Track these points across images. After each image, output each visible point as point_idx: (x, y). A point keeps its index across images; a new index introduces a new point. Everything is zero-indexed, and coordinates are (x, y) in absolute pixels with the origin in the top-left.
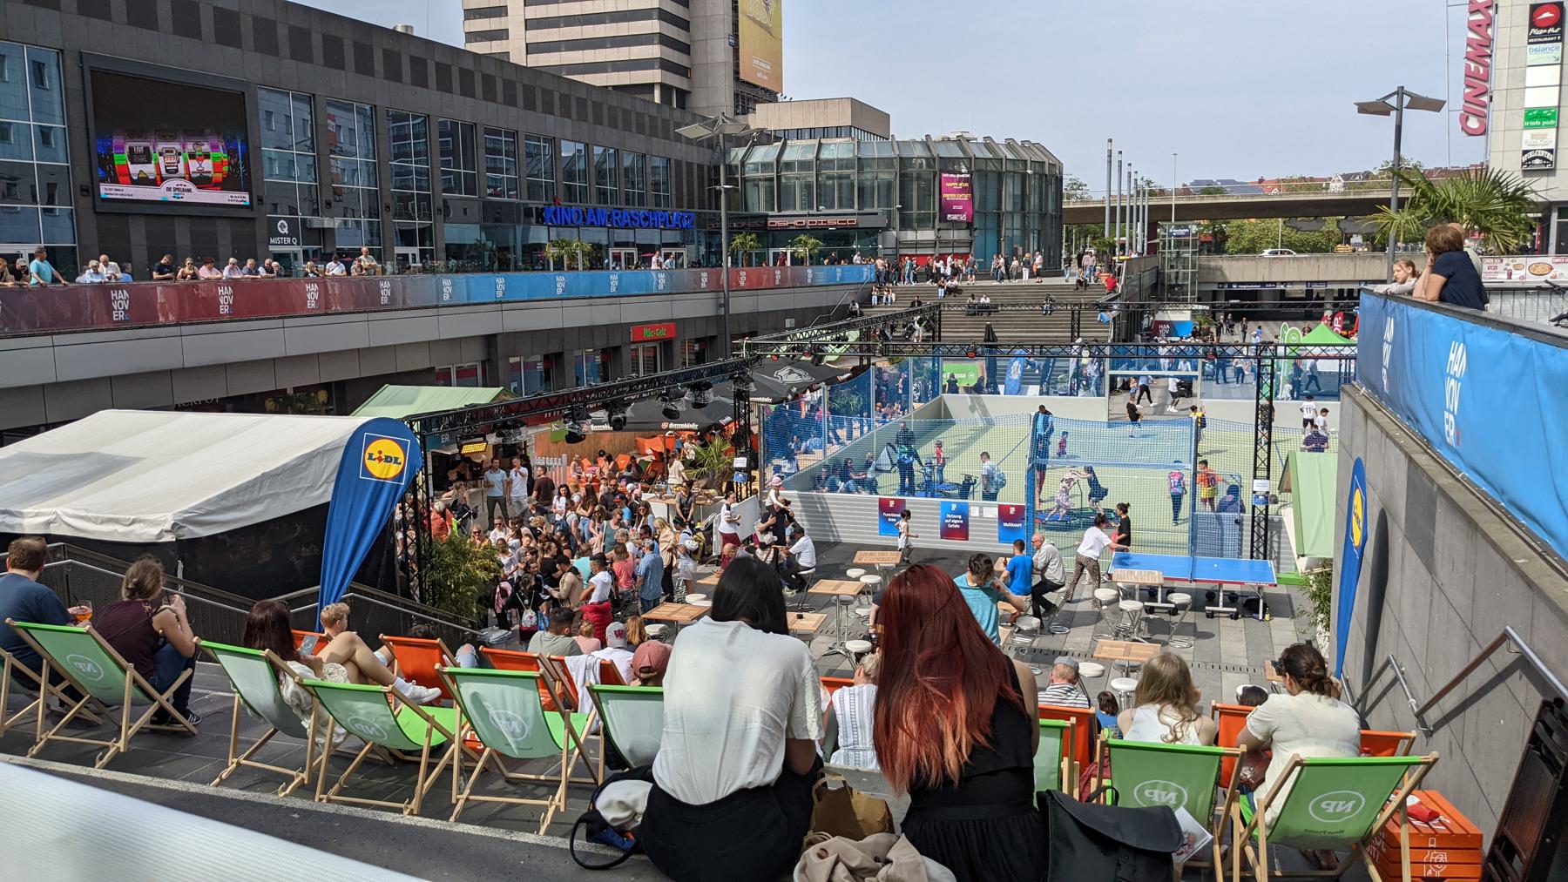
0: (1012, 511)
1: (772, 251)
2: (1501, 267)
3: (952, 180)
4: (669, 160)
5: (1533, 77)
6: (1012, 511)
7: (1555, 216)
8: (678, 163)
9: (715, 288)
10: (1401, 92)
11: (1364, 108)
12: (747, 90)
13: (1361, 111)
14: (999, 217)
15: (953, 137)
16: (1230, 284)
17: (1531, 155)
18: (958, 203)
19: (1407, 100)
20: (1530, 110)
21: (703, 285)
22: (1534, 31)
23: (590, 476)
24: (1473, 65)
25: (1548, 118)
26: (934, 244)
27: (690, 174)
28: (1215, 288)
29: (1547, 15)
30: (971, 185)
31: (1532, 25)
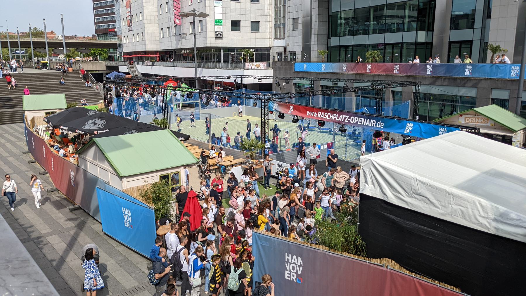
7: (222, 51)
20: (216, 20)
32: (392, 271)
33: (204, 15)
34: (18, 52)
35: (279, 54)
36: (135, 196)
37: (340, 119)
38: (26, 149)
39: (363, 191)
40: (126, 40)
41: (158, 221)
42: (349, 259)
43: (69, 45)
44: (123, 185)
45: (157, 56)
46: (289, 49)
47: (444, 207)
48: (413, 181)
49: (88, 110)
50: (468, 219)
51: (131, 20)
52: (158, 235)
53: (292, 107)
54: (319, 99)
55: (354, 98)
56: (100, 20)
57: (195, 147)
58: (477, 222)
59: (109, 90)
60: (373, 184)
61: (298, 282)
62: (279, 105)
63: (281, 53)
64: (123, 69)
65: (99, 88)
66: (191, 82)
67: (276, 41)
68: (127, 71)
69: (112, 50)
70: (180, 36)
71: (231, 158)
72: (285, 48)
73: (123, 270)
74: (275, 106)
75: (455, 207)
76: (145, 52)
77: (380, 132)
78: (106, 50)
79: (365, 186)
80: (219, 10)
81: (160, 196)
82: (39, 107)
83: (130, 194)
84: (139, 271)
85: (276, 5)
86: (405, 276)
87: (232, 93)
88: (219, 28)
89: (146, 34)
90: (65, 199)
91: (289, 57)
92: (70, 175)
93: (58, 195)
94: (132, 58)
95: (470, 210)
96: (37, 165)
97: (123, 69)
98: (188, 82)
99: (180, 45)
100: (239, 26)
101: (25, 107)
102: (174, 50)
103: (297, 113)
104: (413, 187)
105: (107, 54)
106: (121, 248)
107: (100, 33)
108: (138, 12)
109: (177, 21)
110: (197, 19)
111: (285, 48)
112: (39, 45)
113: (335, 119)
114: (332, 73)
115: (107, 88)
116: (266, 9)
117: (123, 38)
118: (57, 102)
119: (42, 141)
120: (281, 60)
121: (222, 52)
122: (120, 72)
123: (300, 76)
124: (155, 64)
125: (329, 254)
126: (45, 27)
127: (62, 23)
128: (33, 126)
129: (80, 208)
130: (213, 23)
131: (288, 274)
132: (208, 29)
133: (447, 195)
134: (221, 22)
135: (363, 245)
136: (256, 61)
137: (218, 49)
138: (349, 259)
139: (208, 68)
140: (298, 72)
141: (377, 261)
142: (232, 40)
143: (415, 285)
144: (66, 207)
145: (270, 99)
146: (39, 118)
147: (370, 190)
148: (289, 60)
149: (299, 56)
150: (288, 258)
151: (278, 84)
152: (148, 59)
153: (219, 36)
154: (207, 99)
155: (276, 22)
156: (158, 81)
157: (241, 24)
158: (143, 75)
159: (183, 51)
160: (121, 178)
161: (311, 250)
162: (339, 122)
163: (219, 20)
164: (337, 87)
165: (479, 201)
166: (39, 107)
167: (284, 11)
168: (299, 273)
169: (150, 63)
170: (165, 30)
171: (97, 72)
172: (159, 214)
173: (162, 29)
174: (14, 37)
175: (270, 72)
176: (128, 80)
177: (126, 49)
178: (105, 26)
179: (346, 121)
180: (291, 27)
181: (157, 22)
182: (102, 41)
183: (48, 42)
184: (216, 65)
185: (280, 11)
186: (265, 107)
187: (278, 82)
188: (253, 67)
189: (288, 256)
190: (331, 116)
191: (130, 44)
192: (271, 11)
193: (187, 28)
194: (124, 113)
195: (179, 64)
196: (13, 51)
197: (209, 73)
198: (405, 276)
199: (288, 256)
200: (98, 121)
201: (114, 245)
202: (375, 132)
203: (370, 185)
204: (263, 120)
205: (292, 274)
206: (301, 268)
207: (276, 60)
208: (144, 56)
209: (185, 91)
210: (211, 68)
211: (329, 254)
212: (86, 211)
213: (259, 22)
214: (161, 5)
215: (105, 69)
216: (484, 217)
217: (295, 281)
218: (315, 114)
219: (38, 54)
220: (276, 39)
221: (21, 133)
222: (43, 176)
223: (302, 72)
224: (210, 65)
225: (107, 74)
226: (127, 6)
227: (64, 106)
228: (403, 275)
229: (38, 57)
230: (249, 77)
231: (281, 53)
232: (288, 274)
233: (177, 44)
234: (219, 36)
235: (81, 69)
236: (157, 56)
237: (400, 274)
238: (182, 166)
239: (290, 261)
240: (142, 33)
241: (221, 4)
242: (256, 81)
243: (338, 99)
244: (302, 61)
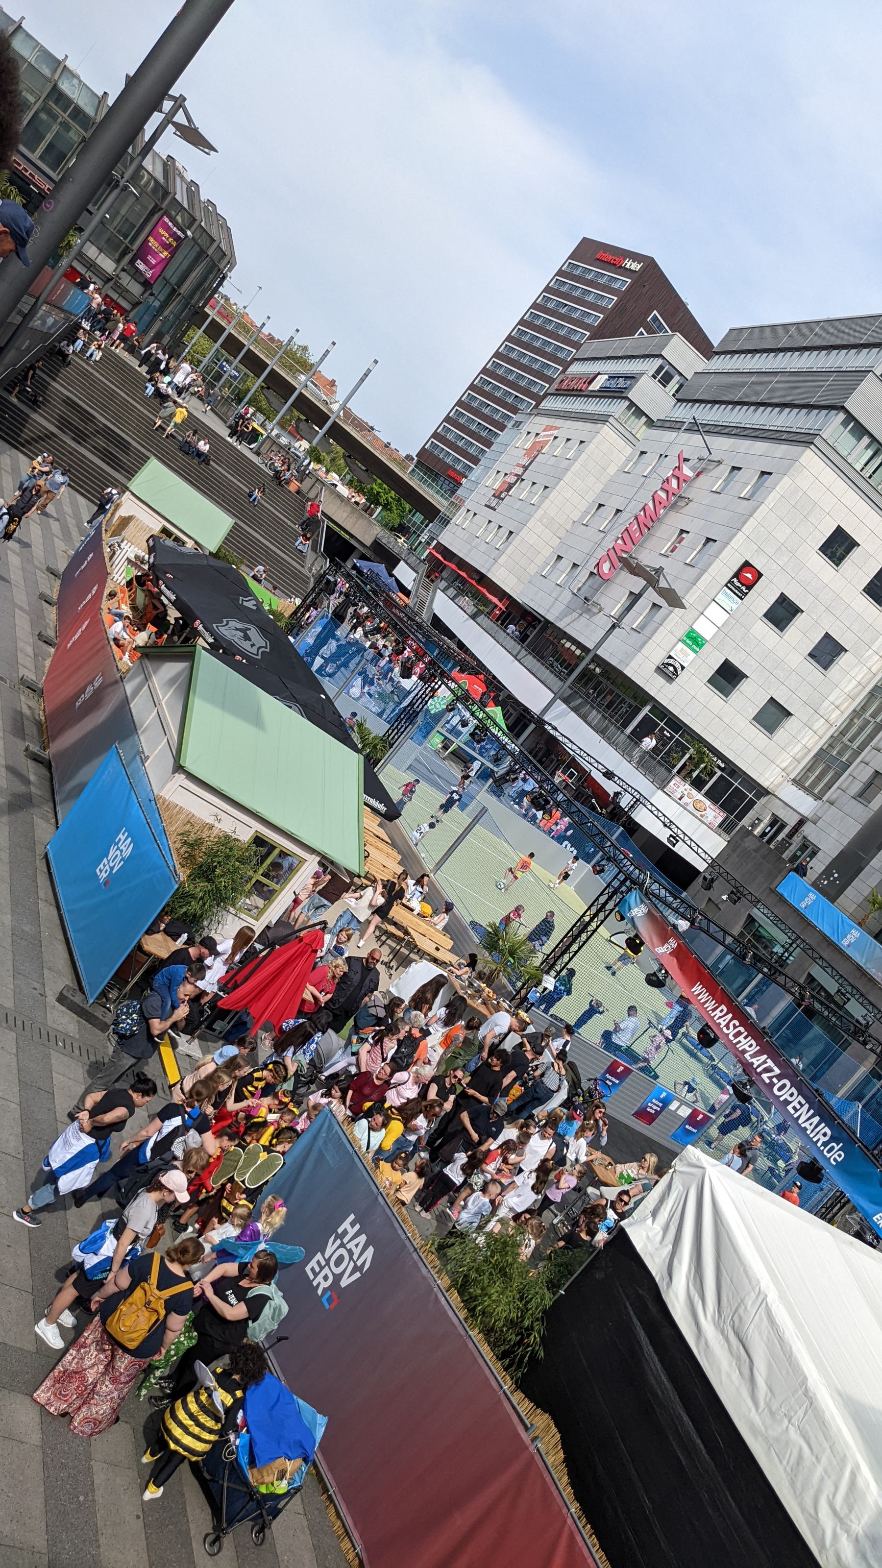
3: (167, 229)
7: (648, 708)
17: (671, 661)
20: (693, 631)
22: (735, 580)
23: (685, 1112)
25: (698, 645)
26: (108, 279)
29: (749, 576)
30: (178, 247)
31: (737, 575)
32: (537, 1458)
33: (674, 600)
34: (227, 367)
35: (776, 823)
36: (170, 829)
37: (756, 1062)
38: (61, 566)
39: (631, 1224)
40: (465, 519)
41: (167, 919)
42: (471, 1345)
43: (337, 433)
44: (170, 784)
45: (500, 605)
46: (808, 830)
47: (772, 1414)
48: (753, 1295)
49: (247, 592)
50: (798, 1485)
51: (510, 487)
52: (139, 947)
53: (673, 944)
54: (777, 1002)
55: (862, 1071)
56: (450, 437)
57: (395, 853)
58: (812, 1512)
59: (330, 588)
60: (666, 1229)
61: (324, 1300)
62: (650, 914)
63: (783, 826)
64: (405, 574)
65: (315, 564)
66: (520, 718)
67: (794, 788)
68: (409, 585)
69: (418, 518)
70: (586, 603)
71: (448, 943)
72: (801, 822)
73: (10, 956)
74: (638, 911)
75: (794, 1435)
76: (482, 579)
77: (820, 1169)
78: (408, 506)
79: (645, 1220)
80: (720, 617)
81: (218, 871)
82: (164, 505)
83: (165, 816)
84: (37, 985)
85: (864, 708)
86: (555, 1493)
87: (596, 820)
88: (683, 655)
89: (516, 540)
90: (39, 724)
91: (793, 848)
92: (91, 682)
93: (32, 703)
94: (445, 567)
95: (819, 1470)
96: (52, 614)
97: (405, 574)
98: (515, 715)
99: (567, 620)
100: (735, 687)
101: (137, 484)
102: (547, 622)
103: (672, 965)
104: (741, 1311)
105: (402, 517)
106: (48, 912)
107: (427, 462)
108: (542, 481)
109: (606, 567)
110: (651, 596)
111: (801, 822)
112: (279, 386)
113: (744, 1052)
114: (859, 968)
115: (328, 581)
116: (831, 698)
117: (463, 510)
118: (206, 525)
119: (103, 575)
120: (769, 841)
121: (646, 710)
122: (391, 575)
123: (779, 911)
124: (479, 619)
125: (440, 1295)
126: (322, 359)
127: (362, 380)
128: (117, 532)
129: (48, 765)
130: (681, 632)
131: (318, 1262)
132: (657, 637)
133: (800, 1393)
134: (700, 646)
135: (534, 1354)
136: (707, 795)
137: (642, 697)
138: (471, 1345)
139: (584, 718)
140: (781, 899)
141: (525, 1406)
142: (690, 700)
143: (559, 1535)
144: (24, 739)
145: (641, 885)
146: (143, 528)
147: (648, 1237)
148: (787, 855)
149: (817, 866)
150: (349, 1228)
151: (708, 885)
152: (477, 596)
153: (668, 671)
154: (508, 773)
155: (831, 746)
156: (446, 654)
157: (744, 686)
158: (436, 622)
159: (563, 641)
160: (179, 768)
161: (392, 1226)
162: (747, 1067)
163: (700, 636)
164: (841, 1007)
165: (858, 1466)
166: (164, 505)
167: (871, 737)
168: (344, 1282)
169: (471, 609)
170: (566, 564)
171: (347, 537)
172: (181, 907)
173: (500, 527)
174: (247, 332)
175: (715, 844)
176: (390, 603)
177: (449, 538)
178: (450, 456)
179: (765, 1076)
180: (856, 787)
181: (562, 533)
182: (414, 483)
183: (301, 394)
184: (607, 728)
185: (861, 729)
186: (615, 893)
187: (712, 881)
188: (686, 800)
189: (353, 1224)
190: (741, 1038)
191: (465, 534)
192: (837, 712)
193: (613, 600)
194: (318, 662)
195: (530, 660)
196: (217, 357)
197: (573, 730)
198: (555, 1493)
199: (353, 1224)
200: (253, 633)
201: (41, 894)
202: (807, 1160)
203: (658, 1227)
204: (587, 919)
205: (326, 1270)
206: (358, 1275)
207: (757, 831)
208: (472, 584)
209: (477, 718)
210: (589, 724)
211: (440, 1295)
212: (55, 779)
213: (789, 714)
214: (600, 505)
215: (368, 542)
216: (835, 1513)
217: (320, 1292)
218: (710, 1005)
219: (264, 404)
220: (798, 782)
221: (81, 531)
222: (41, 643)
223: (791, 906)
224: (595, 716)
225: (363, 557)
226: (528, 452)
227: (212, 544)
228: (553, 1488)
229: (259, 409)
230: (657, 812)
231: (783, 826)
232: (318, 1262)
233: (563, 615)
234: (668, 671)
235: (317, 502)
236: (500, 605)
237: (548, 1479)
238: (318, 853)
239: (345, 1240)
240: (511, 533)
241: (735, 607)
242: (663, 835)
243: (827, 1045)
244: (815, 885)
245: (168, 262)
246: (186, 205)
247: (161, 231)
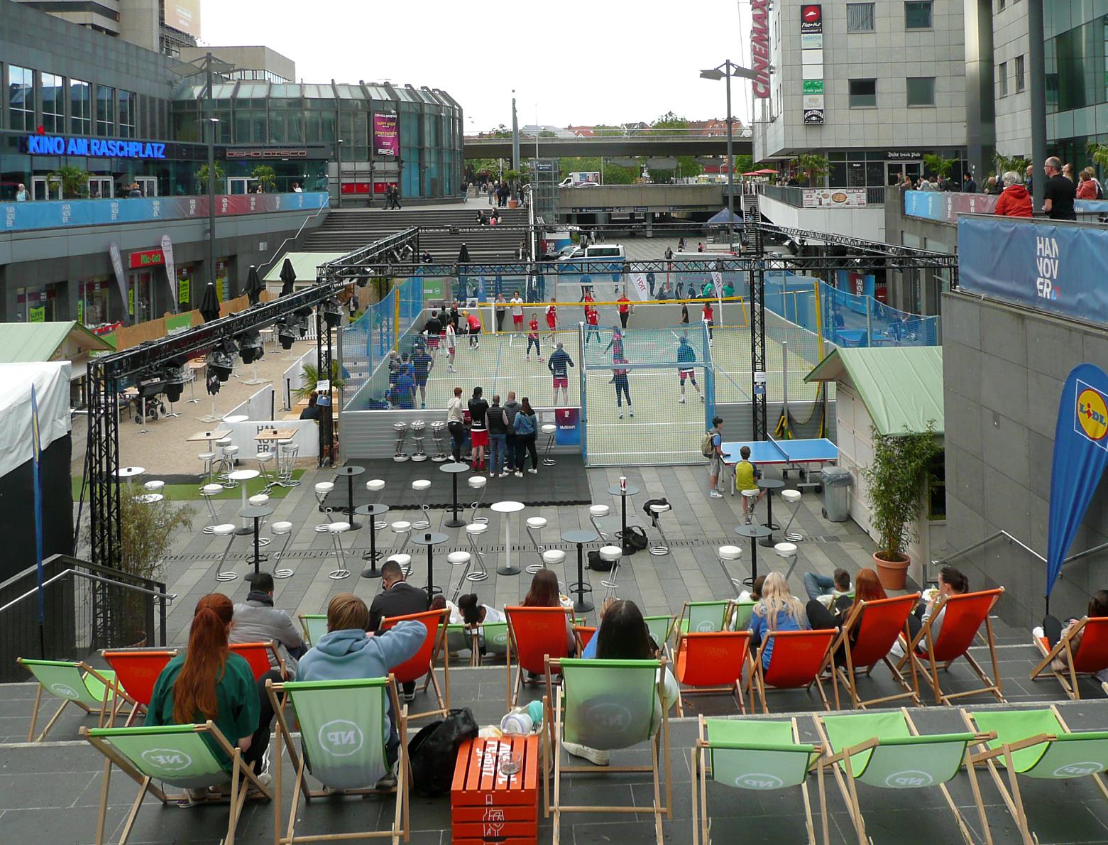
0: (567, 414)
1: (230, 179)
2: (815, 195)
4: (134, 94)
5: (807, 56)
6: (567, 414)
8: (143, 98)
9: (200, 215)
10: (728, 64)
11: (706, 74)
12: (171, 35)
13: (702, 76)
14: (421, 150)
15: (382, 82)
16: (581, 209)
17: (809, 114)
18: (387, 140)
19: (733, 70)
20: (807, 81)
21: (192, 212)
24: (758, 46)
25: (818, 87)
27: (152, 108)
28: (570, 212)
29: (812, 13)
30: (398, 124)
31: (803, 19)
80: (818, 56)
157: (879, 87)
163: (813, 80)
188: (824, 201)
245: (398, 137)
246: (411, 100)
247: (379, 124)
